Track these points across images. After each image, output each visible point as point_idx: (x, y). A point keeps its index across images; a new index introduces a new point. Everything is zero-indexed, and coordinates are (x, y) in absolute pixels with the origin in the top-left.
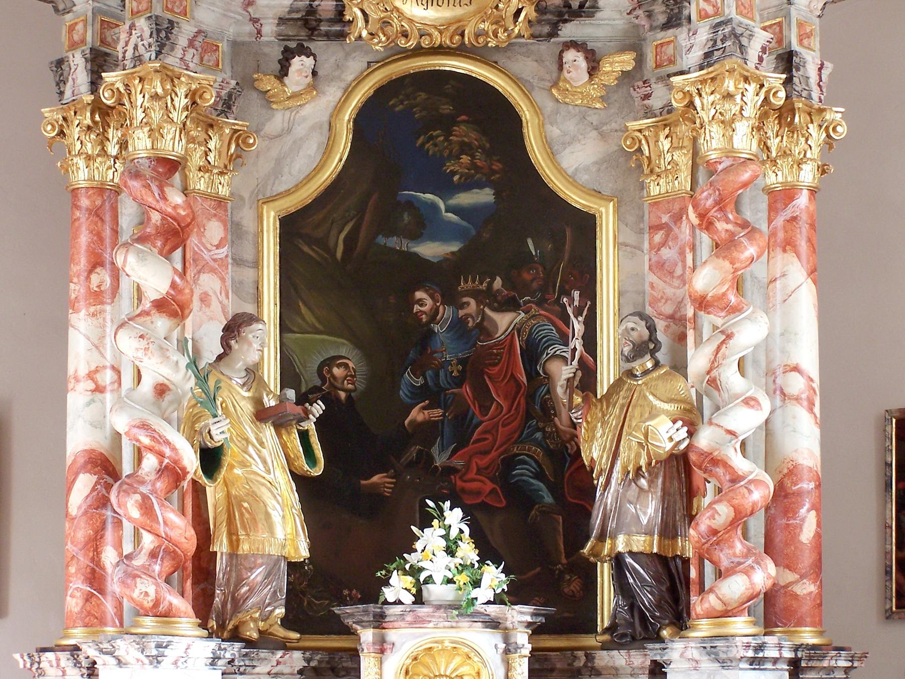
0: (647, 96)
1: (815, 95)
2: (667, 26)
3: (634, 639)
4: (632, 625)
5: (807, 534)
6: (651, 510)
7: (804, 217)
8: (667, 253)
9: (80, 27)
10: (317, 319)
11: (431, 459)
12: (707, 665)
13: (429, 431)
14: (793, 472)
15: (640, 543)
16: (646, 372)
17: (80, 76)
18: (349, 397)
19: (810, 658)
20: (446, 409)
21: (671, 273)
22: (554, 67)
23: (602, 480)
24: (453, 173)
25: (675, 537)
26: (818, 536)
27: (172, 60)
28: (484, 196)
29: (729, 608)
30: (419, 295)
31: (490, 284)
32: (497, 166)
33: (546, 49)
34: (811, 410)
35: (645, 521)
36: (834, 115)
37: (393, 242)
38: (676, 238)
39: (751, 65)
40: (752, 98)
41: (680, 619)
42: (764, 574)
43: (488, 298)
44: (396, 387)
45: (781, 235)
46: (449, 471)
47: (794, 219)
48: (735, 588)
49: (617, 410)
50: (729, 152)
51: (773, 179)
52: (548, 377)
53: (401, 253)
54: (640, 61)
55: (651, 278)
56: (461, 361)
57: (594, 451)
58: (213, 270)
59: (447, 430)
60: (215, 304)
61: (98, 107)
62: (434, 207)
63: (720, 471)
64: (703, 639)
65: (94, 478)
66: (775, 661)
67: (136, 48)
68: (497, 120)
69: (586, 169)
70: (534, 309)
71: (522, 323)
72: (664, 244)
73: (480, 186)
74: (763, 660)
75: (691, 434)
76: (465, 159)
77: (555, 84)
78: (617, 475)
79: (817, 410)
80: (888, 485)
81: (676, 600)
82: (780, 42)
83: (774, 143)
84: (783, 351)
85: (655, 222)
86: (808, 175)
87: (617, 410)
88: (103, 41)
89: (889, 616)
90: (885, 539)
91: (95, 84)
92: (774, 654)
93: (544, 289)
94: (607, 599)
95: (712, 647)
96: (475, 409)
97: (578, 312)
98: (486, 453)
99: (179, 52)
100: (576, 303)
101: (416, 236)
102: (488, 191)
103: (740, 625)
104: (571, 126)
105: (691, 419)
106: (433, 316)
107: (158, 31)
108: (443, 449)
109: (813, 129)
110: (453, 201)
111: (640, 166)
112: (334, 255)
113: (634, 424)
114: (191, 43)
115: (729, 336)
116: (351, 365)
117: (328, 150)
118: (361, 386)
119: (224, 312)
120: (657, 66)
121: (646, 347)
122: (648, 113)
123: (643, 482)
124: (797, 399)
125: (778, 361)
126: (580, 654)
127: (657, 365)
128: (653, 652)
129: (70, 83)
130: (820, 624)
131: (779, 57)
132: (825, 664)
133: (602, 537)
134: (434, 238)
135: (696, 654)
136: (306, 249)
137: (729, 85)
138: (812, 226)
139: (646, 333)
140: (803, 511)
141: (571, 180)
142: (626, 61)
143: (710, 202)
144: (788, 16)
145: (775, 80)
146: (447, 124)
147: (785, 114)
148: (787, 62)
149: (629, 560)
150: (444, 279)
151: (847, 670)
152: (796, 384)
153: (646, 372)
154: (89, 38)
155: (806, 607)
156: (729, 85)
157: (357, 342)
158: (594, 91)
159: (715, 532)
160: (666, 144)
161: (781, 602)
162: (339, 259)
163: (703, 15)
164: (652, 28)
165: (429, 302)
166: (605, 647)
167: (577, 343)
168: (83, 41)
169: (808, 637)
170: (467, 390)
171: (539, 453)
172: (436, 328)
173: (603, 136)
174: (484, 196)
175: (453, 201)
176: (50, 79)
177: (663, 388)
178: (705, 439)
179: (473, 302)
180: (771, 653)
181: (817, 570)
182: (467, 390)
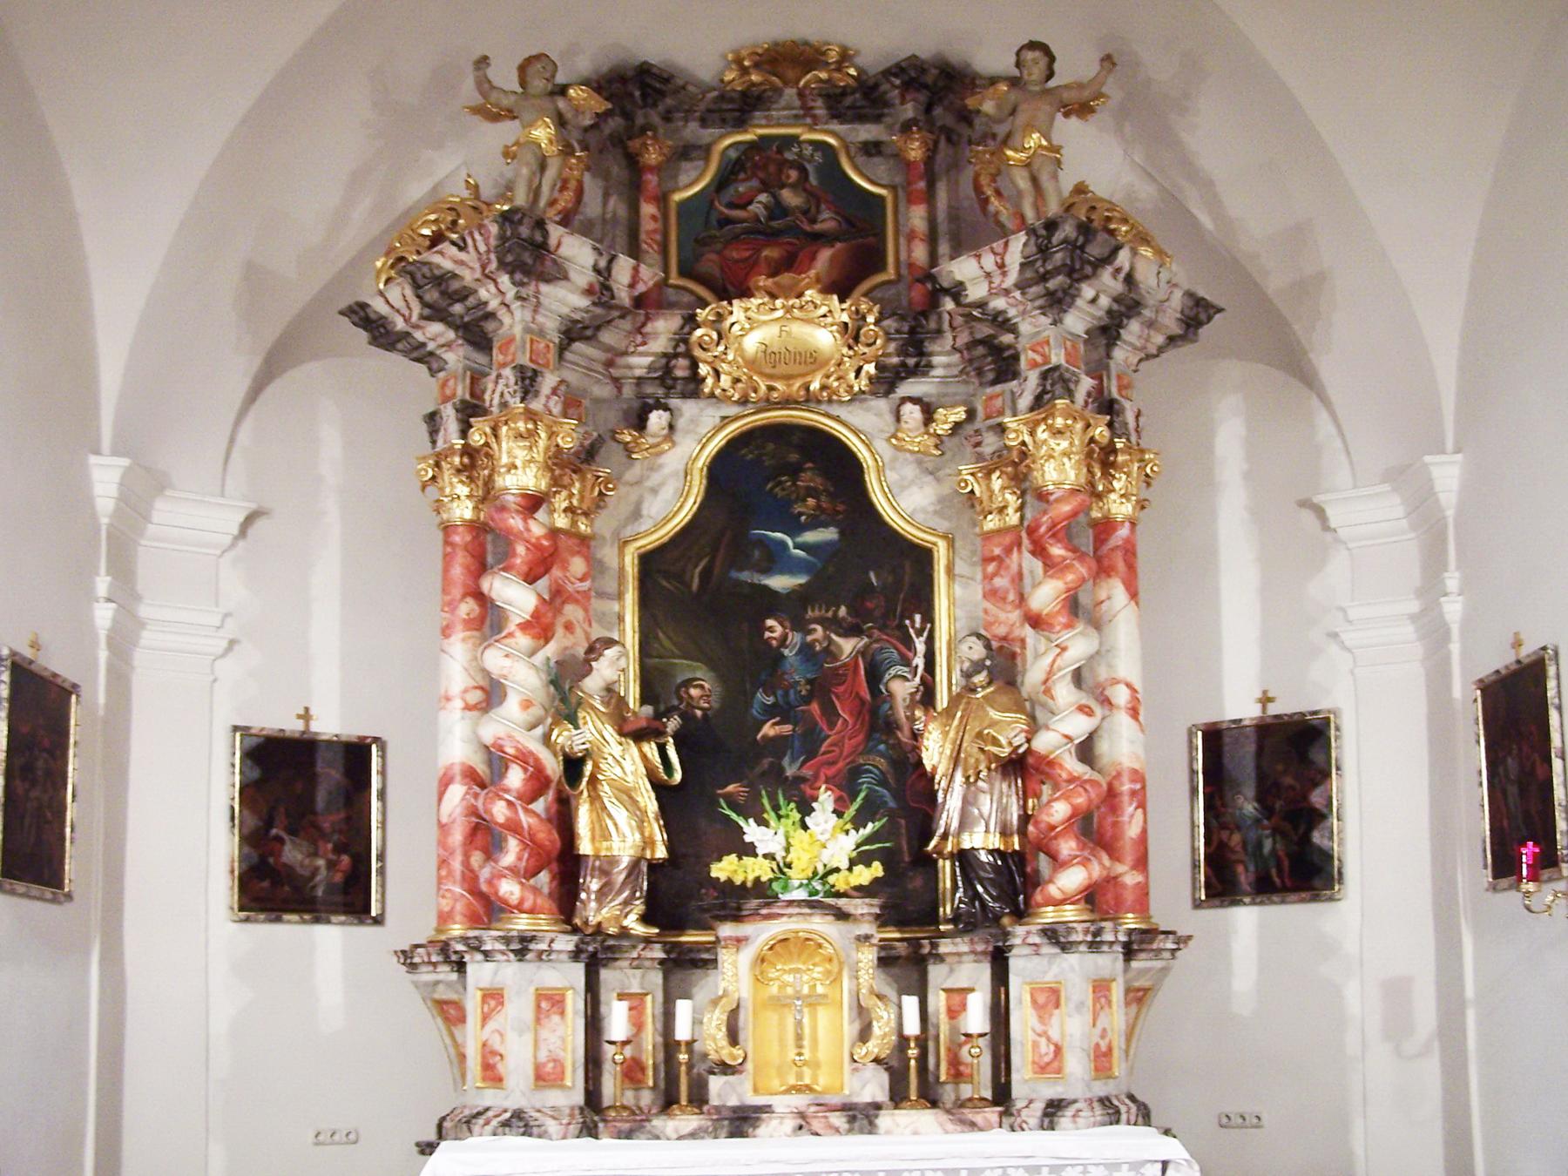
0: (978, 444)
8: (999, 582)
9: (451, 383)
10: (675, 644)
11: (782, 770)
12: (1049, 950)
13: (778, 746)
17: (451, 424)
18: (705, 716)
19: (1142, 942)
20: (795, 725)
21: (1004, 599)
22: (890, 418)
23: (944, 784)
24: (801, 514)
27: (537, 405)
28: (828, 534)
29: (1021, 934)
30: (770, 622)
31: (835, 613)
32: (841, 508)
33: (882, 405)
37: (746, 576)
38: (1008, 568)
43: (833, 624)
44: (748, 704)
46: (799, 780)
52: (891, 695)
53: (752, 585)
56: (809, 682)
58: (577, 601)
59: (797, 744)
60: (579, 631)
61: (468, 451)
62: (783, 544)
65: (464, 788)
66: (1111, 943)
67: (502, 395)
68: (841, 468)
69: (924, 511)
70: (876, 633)
71: (867, 646)
72: (995, 575)
73: (825, 525)
76: (811, 501)
80: (1194, 791)
85: (988, 554)
88: (472, 395)
91: (464, 434)
93: (885, 616)
96: (822, 724)
98: (834, 763)
99: (542, 399)
100: (918, 625)
101: (768, 571)
102: (832, 529)
106: (783, 641)
107: (523, 379)
108: (793, 760)
110: (799, 539)
112: (689, 586)
114: (554, 391)
116: (707, 686)
117: (683, 495)
118: (716, 705)
119: (588, 638)
120: (988, 417)
129: (441, 433)
132: (1155, 946)
134: (782, 572)
135: (1037, 939)
136: (665, 583)
142: (959, 414)
144: (1107, 368)
146: (795, 471)
150: (793, 608)
151: (1173, 951)
154: (459, 392)
157: (712, 665)
162: (693, 589)
163: (1034, 365)
165: (779, 629)
168: (454, 395)
170: (815, 707)
171: (882, 763)
172: (786, 652)
174: (828, 534)
175: (799, 539)
176: (424, 428)
179: (819, 628)
180: (1108, 937)
182: (815, 707)
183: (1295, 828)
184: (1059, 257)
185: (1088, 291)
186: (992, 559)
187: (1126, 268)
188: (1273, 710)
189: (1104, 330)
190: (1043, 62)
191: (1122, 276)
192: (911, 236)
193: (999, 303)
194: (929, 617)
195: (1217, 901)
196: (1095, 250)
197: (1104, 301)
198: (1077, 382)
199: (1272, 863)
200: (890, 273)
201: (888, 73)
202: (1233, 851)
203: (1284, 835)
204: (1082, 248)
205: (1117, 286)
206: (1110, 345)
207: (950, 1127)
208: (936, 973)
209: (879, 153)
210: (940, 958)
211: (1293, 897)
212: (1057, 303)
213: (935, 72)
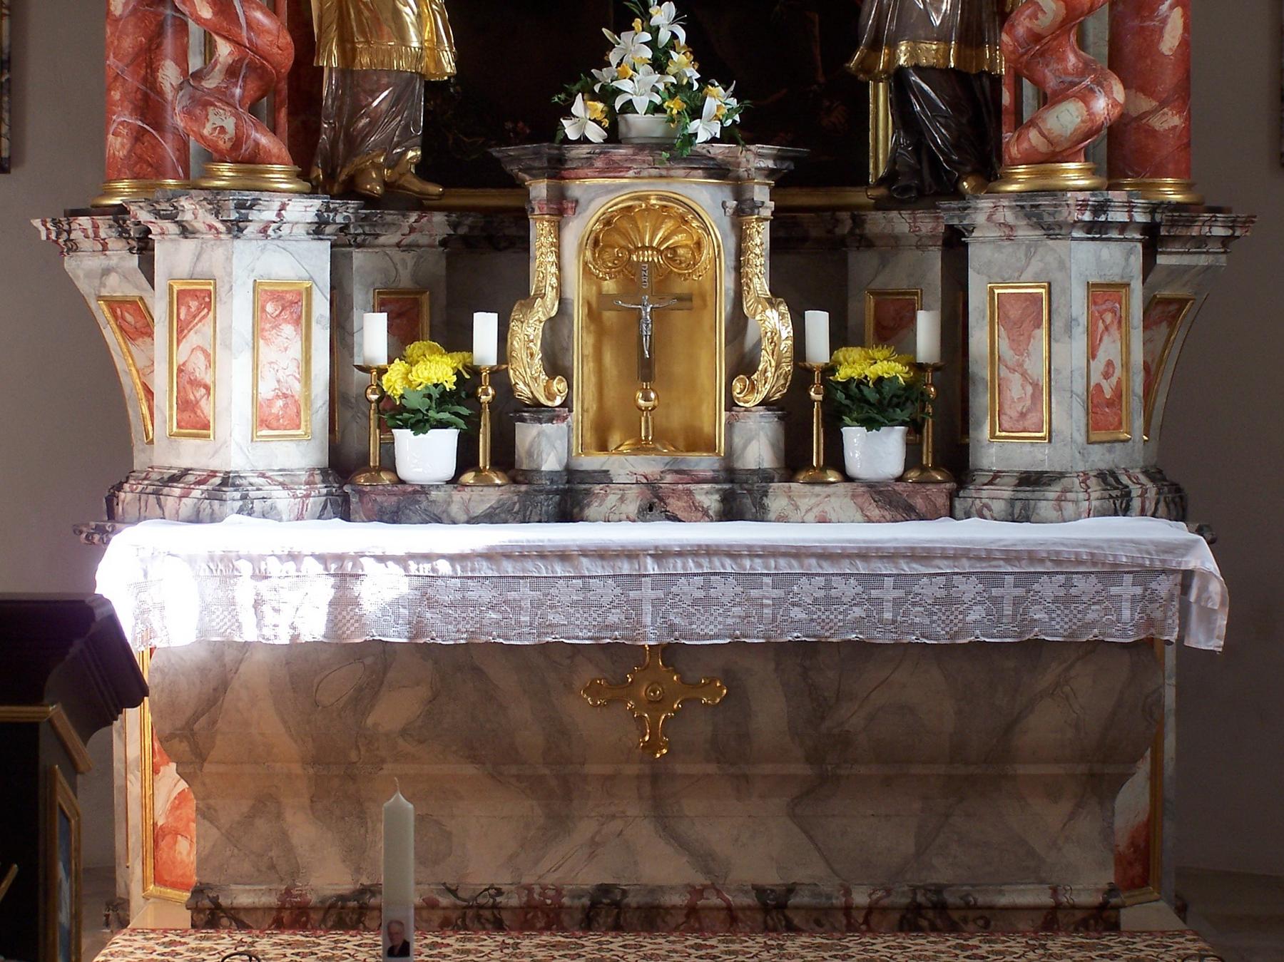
3: (921, 194)
4: (917, 173)
12: (1025, 233)
15: (930, 52)
26: (1185, 43)
48: (1066, 118)
66: (1123, 227)
74: (1107, 226)
92: (1121, 217)
103: (1073, 174)
126: (845, 216)
128: (948, 214)
133: (875, 46)
135: (1008, 216)
151: (1225, 241)
166: (880, 205)
181: (1183, 95)
207: (876, 512)
210: (867, 243)
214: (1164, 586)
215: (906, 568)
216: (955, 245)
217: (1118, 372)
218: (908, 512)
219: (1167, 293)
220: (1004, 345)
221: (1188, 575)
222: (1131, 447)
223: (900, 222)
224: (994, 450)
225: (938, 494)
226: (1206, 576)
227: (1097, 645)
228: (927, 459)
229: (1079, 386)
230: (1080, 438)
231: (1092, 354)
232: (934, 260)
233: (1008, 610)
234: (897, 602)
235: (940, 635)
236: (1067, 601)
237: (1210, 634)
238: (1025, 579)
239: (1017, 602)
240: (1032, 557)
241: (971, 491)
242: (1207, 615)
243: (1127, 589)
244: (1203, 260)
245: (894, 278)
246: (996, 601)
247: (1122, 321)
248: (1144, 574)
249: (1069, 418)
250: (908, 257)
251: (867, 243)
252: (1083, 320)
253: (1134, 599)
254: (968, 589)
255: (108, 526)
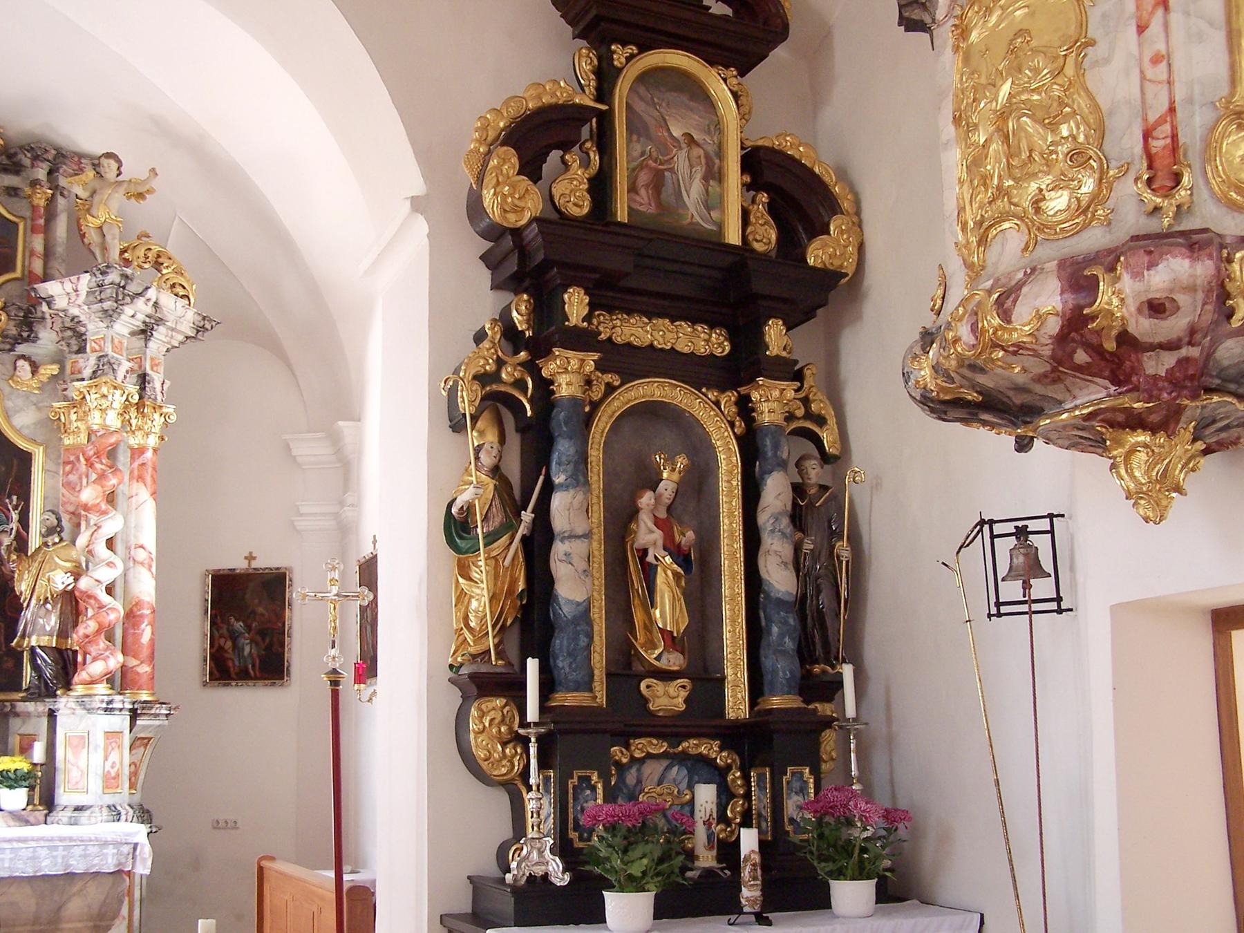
0: (65, 390)
1: (159, 397)
2: (78, 352)
3: (40, 695)
4: (39, 688)
5: (146, 637)
6: (53, 623)
7: (150, 464)
8: (72, 478)
12: (80, 712)
14: (139, 604)
15: (45, 641)
16: (55, 544)
22: (11, 368)
25: (67, 638)
26: (152, 640)
34: (150, 570)
35: (48, 628)
36: (169, 409)
39: (119, 379)
40: (118, 400)
41: (68, 686)
42: (115, 661)
45: (136, 473)
47: (143, 464)
48: (97, 668)
49: (36, 565)
50: (104, 427)
51: (134, 441)
54: (62, 369)
55: (63, 490)
57: (22, 587)
63: (92, 601)
64: (78, 697)
66: (121, 710)
69: (28, 427)
72: (70, 472)
74: (112, 709)
75: (76, 580)
77: (11, 378)
78: (34, 602)
79: (154, 569)
81: (67, 674)
82: (140, 367)
83: (134, 422)
84: (135, 537)
86: (152, 441)
87: (36, 565)
89: (205, 684)
90: (204, 642)
92: (120, 706)
94: (28, 673)
95: (81, 701)
97: (15, 508)
103: (102, 689)
104: (20, 402)
105: (77, 574)
109: (156, 416)
111: (59, 428)
113: (1218, 381)
115: (99, 527)
121: (50, 531)
122: (66, 399)
123: (49, 606)
124: (142, 564)
125: (133, 542)
126: (8, 704)
127: (61, 540)
128: (49, 704)
130: (152, 689)
131: (139, 376)
132: (153, 711)
133: (23, 636)
135: (73, 705)
137: (104, 390)
138: (154, 469)
139: (56, 522)
140: (143, 626)
141: (18, 432)
142: (54, 369)
143: (91, 453)
144: (145, 354)
145: (133, 389)
147: (140, 406)
148: (143, 379)
149: (39, 650)
151: (167, 715)
152: (141, 555)
153: (55, 544)
155: (144, 679)
156: (104, 390)
158: (34, 383)
159: (87, 636)
160: (74, 417)
161: (130, 676)
163: (94, 351)
164: (70, 352)
166: (23, 700)
167: (14, 525)
169: (145, 696)
173: (39, 409)
177: (64, 553)
178: (84, 583)
181: (152, 658)
183: (263, 639)
184: (109, 292)
185: (128, 310)
186: (69, 463)
187: (154, 300)
188: (255, 564)
189: (143, 332)
190: (114, 165)
191: (151, 303)
192: (32, 253)
193: (74, 311)
194: (25, 497)
195: (216, 683)
196: (133, 288)
197: (140, 317)
198: (119, 364)
199: (249, 661)
200: (18, 274)
201: (22, 148)
202: (226, 651)
203: (257, 644)
204: (124, 287)
205: (149, 309)
206: (147, 340)
207: (12, 823)
208: (15, 723)
209: (16, 195)
210: (17, 715)
211: (261, 682)
212: (109, 316)
213: (54, 152)
214: (126, 849)
215: (15, 845)
216: (52, 715)
217: (118, 766)
218: (27, 822)
219: (142, 735)
220: (70, 756)
221: (136, 845)
222: (123, 796)
223: (30, 707)
224: (64, 797)
225: (40, 815)
226: (143, 845)
227: (97, 873)
228: (36, 801)
229: (100, 772)
230: (100, 791)
231: (106, 759)
232: (45, 721)
233: (60, 860)
234: (11, 859)
235: (30, 872)
236: (85, 856)
237: (144, 868)
238: (67, 848)
239: (64, 857)
240: (71, 839)
241: (54, 813)
242: (144, 860)
243: (111, 850)
244: (157, 723)
245: (28, 729)
246: (55, 857)
247: (120, 747)
248: (118, 844)
249: (96, 784)
250: (34, 720)
251: (17, 715)
252: (102, 746)
253: (113, 855)
254: (43, 853)
255: (1217, 240)
